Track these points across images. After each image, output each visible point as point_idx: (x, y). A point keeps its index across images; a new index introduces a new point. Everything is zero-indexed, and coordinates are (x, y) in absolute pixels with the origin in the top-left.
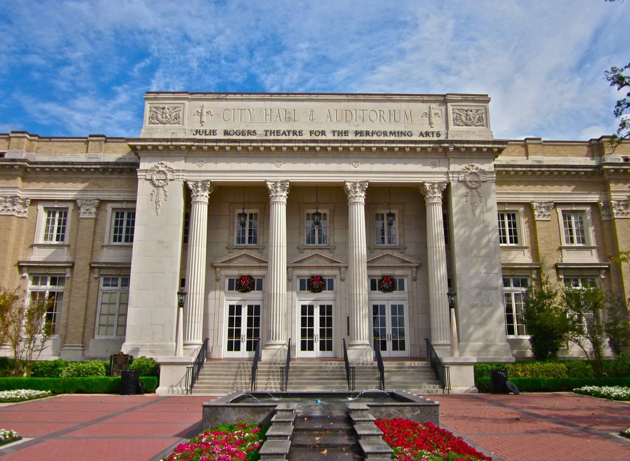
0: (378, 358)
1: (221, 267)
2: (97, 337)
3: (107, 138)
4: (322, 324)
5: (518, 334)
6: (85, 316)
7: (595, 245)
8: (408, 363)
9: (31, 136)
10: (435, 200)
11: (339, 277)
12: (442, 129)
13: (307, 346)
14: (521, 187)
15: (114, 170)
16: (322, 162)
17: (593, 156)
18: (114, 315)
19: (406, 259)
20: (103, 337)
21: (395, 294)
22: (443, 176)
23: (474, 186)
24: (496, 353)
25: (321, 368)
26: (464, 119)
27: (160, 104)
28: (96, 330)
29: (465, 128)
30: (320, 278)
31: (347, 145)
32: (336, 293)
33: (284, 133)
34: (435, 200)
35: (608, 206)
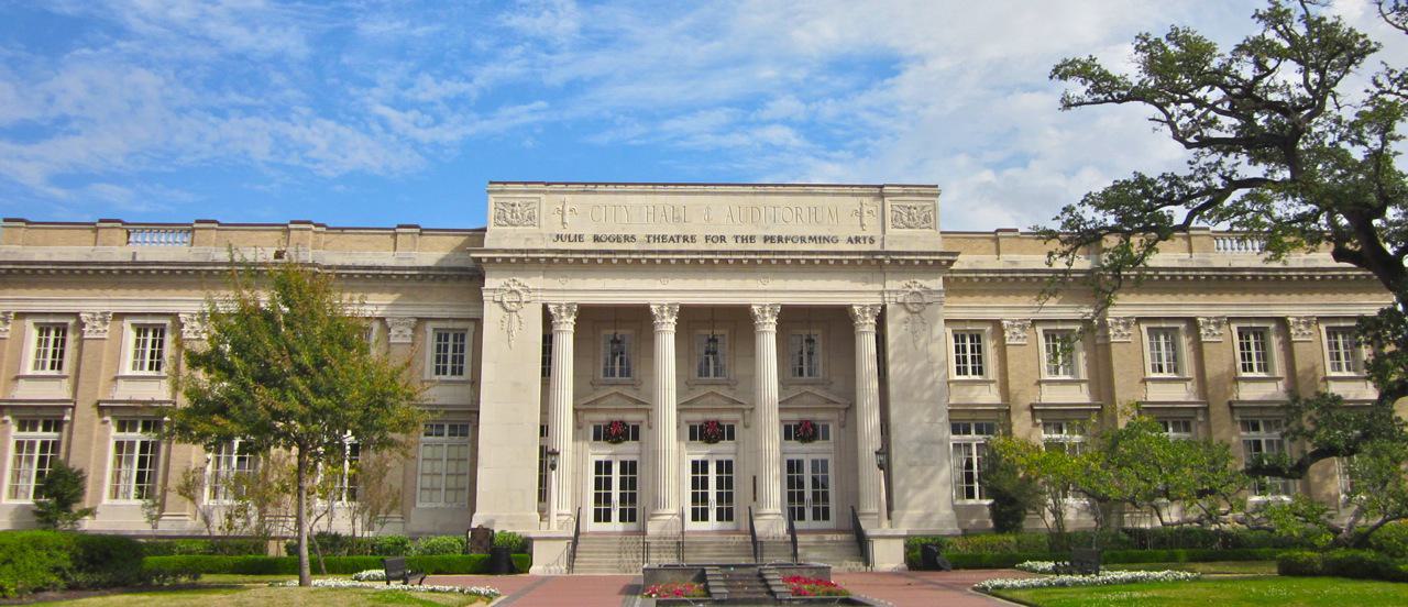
0: (791, 530)
1: (584, 410)
2: (419, 505)
3: (422, 230)
4: (719, 486)
5: (980, 498)
6: (404, 477)
7: (1086, 378)
8: (828, 537)
9: (317, 225)
10: (866, 329)
11: (741, 422)
12: (877, 233)
13: (700, 515)
14: (989, 298)
15: (436, 276)
16: (721, 278)
17: (1089, 254)
18: (441, 474)
19: (831, 398)
20: (426, 505)
21: (818, 445)
22: (875, 295)
23: (918, 309)
24: (940, 523)
25: (722, 543)
26: (905, 219)
27: (509, 198)
28: (418, 496)
29: (907, 230)
30: (718, 424)
31: (753, 257)
32: (737, 444)
33: (672, 239)
34: (866, 329)
35: (1104, 325)
